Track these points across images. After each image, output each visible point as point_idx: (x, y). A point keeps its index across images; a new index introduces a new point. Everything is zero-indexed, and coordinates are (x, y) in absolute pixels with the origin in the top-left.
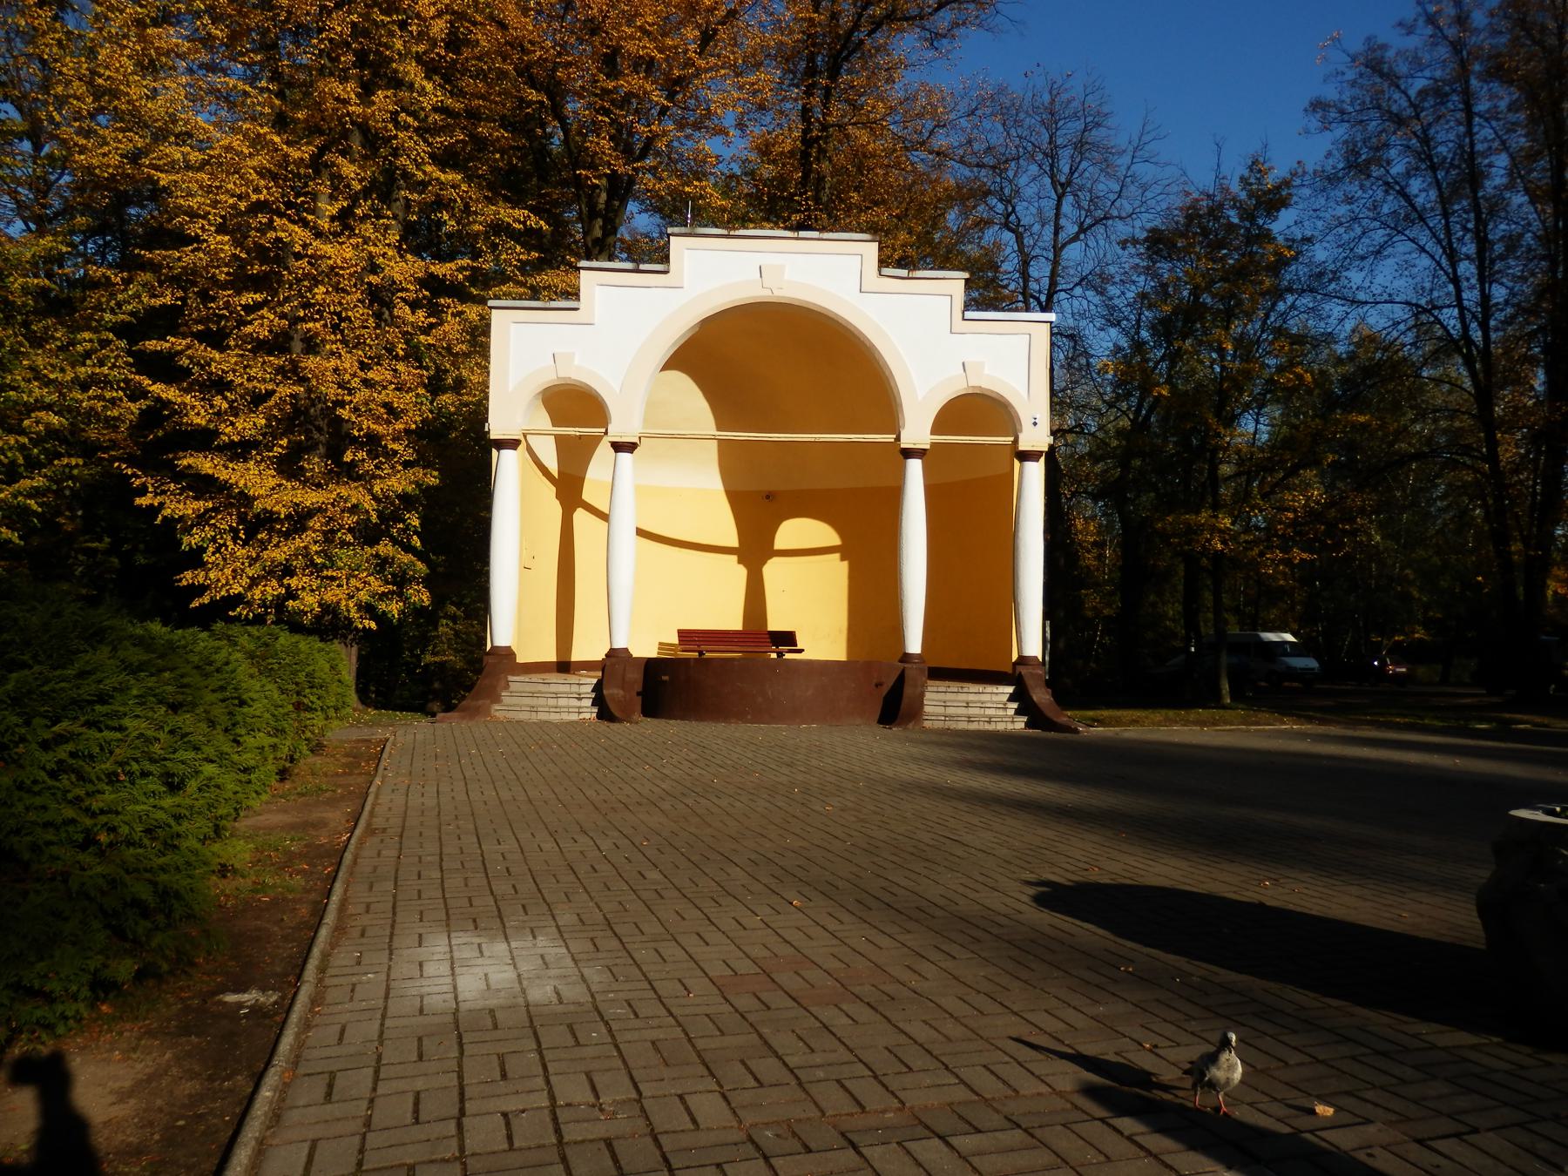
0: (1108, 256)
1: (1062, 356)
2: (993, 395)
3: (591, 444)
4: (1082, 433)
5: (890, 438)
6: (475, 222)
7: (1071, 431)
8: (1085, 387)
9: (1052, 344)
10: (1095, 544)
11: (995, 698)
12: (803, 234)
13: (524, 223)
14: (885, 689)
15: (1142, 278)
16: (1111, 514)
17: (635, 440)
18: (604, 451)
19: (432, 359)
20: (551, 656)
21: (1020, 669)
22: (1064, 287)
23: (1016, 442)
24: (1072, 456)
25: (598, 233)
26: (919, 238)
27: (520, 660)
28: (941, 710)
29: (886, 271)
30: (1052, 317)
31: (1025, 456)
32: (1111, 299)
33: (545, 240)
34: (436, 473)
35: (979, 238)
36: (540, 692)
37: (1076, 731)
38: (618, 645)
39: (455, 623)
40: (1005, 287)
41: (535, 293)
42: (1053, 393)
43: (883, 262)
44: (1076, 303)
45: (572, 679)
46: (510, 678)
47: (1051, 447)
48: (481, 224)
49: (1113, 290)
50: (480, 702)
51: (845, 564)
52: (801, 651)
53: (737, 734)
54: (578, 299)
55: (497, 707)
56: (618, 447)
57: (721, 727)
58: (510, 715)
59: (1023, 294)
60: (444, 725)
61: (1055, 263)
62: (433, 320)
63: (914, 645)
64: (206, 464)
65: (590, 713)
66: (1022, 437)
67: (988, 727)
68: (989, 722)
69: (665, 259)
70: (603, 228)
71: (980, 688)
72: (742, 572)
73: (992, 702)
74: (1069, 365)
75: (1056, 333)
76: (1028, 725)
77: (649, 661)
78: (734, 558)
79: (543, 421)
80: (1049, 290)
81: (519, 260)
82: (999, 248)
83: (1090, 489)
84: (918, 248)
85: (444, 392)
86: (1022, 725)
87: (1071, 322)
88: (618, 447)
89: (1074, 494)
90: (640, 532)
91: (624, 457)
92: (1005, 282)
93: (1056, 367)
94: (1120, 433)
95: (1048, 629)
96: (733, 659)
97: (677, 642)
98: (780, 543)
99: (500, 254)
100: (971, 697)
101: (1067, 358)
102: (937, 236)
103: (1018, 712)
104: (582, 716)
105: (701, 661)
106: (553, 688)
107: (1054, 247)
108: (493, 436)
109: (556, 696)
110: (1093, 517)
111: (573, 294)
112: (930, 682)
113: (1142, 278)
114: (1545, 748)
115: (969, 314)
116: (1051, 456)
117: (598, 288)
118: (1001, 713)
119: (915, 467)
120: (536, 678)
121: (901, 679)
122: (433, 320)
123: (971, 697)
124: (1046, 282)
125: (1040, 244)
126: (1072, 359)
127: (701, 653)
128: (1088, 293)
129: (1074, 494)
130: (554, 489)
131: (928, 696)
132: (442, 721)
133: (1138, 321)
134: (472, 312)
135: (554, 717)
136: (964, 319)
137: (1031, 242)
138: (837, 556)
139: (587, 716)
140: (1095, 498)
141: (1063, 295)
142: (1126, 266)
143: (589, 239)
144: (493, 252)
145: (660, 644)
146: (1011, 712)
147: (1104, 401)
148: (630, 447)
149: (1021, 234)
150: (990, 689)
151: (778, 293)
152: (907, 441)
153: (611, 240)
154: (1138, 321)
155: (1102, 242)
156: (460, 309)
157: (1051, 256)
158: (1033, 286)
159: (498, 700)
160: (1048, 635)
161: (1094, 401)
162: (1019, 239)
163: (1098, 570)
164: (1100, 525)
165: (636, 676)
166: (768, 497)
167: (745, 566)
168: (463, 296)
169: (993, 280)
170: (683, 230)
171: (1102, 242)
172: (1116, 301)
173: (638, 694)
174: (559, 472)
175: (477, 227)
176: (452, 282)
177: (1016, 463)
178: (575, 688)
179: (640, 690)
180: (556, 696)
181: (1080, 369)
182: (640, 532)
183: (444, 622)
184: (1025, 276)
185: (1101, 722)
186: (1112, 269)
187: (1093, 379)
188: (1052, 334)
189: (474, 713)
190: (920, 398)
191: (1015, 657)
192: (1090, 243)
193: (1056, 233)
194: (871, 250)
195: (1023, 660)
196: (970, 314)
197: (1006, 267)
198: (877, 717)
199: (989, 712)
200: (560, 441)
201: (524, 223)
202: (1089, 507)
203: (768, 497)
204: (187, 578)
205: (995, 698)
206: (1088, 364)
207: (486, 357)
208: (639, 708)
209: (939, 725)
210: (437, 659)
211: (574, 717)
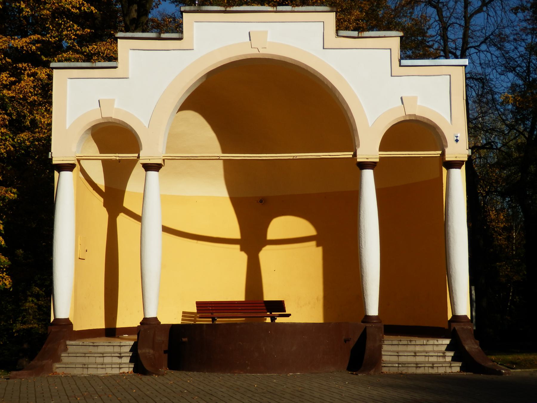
0: (504, 21)
1: (474, 94)
2: (425, 121)
3: (130, 165)
4: (491, 148)
5: (349, 154)
6: (44, 9)
7: (483, 147)
8: (492, 115)
9: (467, 85)
10: (504, 229)
11: (436, 348)
12: (280, 8)
13: (79, 9)
14: (352, 344)
15: (530, 36)
16: (516, 207)
17: (160, 162)
18: (138, 170)
19: (13, 108)
20: (101, 325)
22: (473, 44)
23: (443, 154)
24: (484, 165)
25: (134, 15)
26: (367, 13)
27: (76, 328)
28: (395, 359)
29: (342, 33)
30: (466, 61)
32: (507, 52)
33: (97, 21)
34: (14, 190)
35: (411, 13)
36: (91, 353)
37: (500, 373)
38: (151, 314)
39: (38, 300)
40: (431, 47)
41: (88, 58)
42: (469, 120)
43: (340, 26)
44: (482, 55)
45: (116, 342)
46: (68, 342)
47: (469, 157)
48: (48, 9)
49: (509, 46)
50: (45, 362)
51: (320, 249)
52: (288, 315)
53: (238, 383)
54: (116, 59)
55: (57, 365)
56: (148, 167)
57: (227, 376)
58: (68, 371)
59: (444, 51)
60: (16, 381)
61: (466, 28)
62: (13, 79)
65: (128, 368)
66: (447, 151)
67: (431, 371)
68: (433, 367)
70: (138, 11)
71: (424, 341)
72: (243, 257)
73: (434, 351)
74: (480, 101)
75: (470, 78)
76: (462, 369)
77: (173, 328)
78: (238, 247)
79: (93, 149)
80: (462, 47)
81: (76, 35)
82: (425, 19)
83: (499, 189)
84: (367, 21)
85: (23, 132)
86: (458, 369)
87: (479, 70)
88: (148, 167)
89: (488, 193)
90: (165, 229)
91: (152, 174)
92: (431, 43)
93: (470, 102)
94: (519, 147)
95: (473, 292)
96: (235, 324)
97: (195, 310)
98: (272, 234)
99: (62, 31)
100: (418, 348)
101: (478, 95)
102: (380, 13)
103: (454, 359)
104: (122, 371)
105: (213, 327)
106: (100, 349)
107: (465, 17)
108: (54, 162)
109: (103, 355)
110: (502, 209)
111: (113, 57)
112: (386, 337)
113: (530, 36)
115: (404, 62)
116: (469, 164)
118: (441, 359)
119: (368, 176)
120: (88, 341)
121: (364, 336)
122: (13, 79)
123: (418, 348)
124: (460, 42)
125: (455, 15)
126: (481, 95)
127: (214, 319)
128: (490, 49)
129: (488, 193)
130: (102, 200)
131: (385, 348)
132: (14, 378)
133: (528, 67)
134: (42, 73)
135: (101, 372)
136: (400, 66)
137: (448, 14)
138: (314, 243)
139: (126, 370)
140: (503, 195)
141: (473, 50)
142: (518, 28)
143: (127, 19)
144: (57, 30)
145: (184, 313)
146: (449, 359)
147: (507, 125)
148: (156, 167)
149: (441, 9)
150: (432, 341)
151: (262, 51)
153: (144, 19)
154: (528, 67)
155: (499, 12)
156: (33, 70)
157: (463, 23)
158: (451, 45)
159: (58, 360)
160: (474, 297)
161: (499, 124)
162: (440, 12)
163: (508, 247)
164: (508, 215)
165: (163, 339)
166: (261, 201)
167: (246, 252)
168: (37, 62)
169: (422, 42)
170: (192, 8)
171: (499, 12)
172: (512, 54)
173: (165, 352)
174: (106, 187)
175: (45, 12)
176: (27, 51)
177: (444, 170)
178: (117, 349)
179: (166, 348)
180: (103, 355)
181: (487, 103)
182: (165, 229)
183: (30, 299)
184: (445, 38)
185: (519, 365)
186: (508, 31)
187: (497, 110)
188: (466, 79)
189: (39, 370)
191: (450, 316)
192: (490, 13)
193: (466, 7)
194: (330, 18)
195: (456, 318)
196: (404, 62)
197: (431, 32)
198: (346, 365)
199: (432, 359)
200: (106, 164)
201: (79, 9)
202: (500, 202)
203: (261, 201)
205: (436, 348)
206: (494, 100)
207: (51, 104)
208: (165, 362)
209: (393, 370)
210: (25, 327)
211: (116, 371)
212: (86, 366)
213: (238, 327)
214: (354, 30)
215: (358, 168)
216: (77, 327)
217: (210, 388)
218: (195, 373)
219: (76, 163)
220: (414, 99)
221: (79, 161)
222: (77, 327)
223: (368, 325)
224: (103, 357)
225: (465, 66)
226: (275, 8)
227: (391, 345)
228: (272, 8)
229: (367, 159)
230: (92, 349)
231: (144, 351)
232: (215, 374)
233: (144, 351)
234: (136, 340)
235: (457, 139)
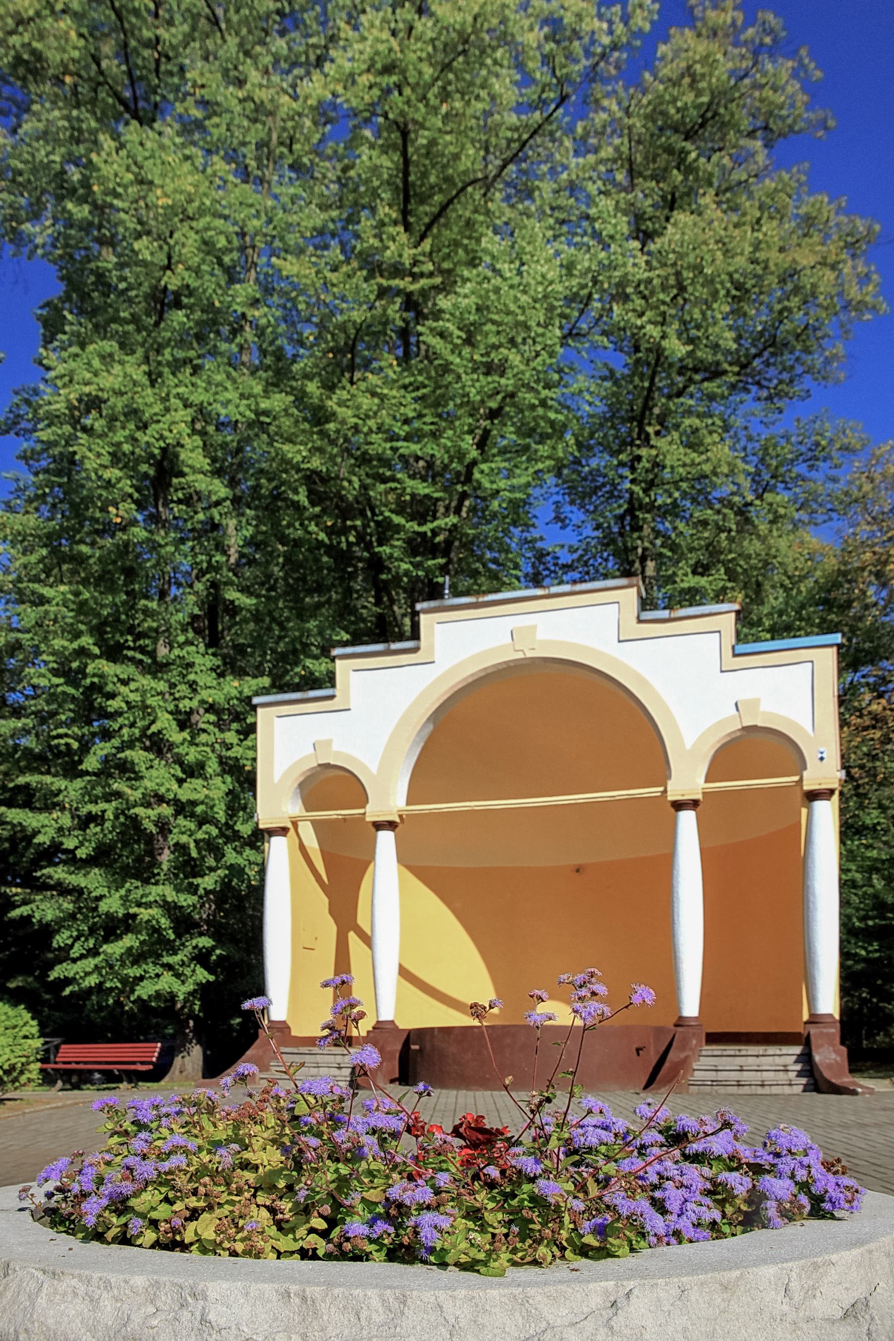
5: (657, 790)
30: (838, 638)
31: (813, 796)
54: (333, 686)
63: (690, 1007)
64: (59, 873)
69: (415, 635)
103: (800, 1074)
111: (330, 679)
136: (640, 621)
151: (530, 654)
152: (374, 811)
178: (339, 1059)
190: (688, 745)
191: (806, 1017)
194: (629, 597)
195: (815, 1019)
200: (317, 825)
204: (56, 973)
214: (665, 608)
215: (672, 810)
219: (290, 825)
220: (756, 702)
221: (295, 824)
230: (307, 1058)
234: (296, 1032)
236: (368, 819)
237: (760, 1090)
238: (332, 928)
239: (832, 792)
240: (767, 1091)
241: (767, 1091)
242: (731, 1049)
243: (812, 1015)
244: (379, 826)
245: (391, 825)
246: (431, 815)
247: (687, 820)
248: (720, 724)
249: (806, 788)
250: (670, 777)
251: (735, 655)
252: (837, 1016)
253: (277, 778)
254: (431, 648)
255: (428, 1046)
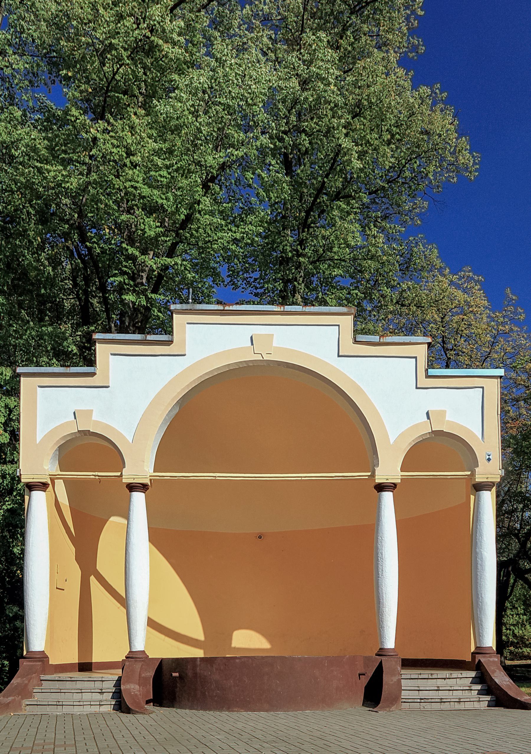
20: (74, 659)
21: (479, 657)
30: (501, 372)
31: (479, 487)
45: (95, 675)
53: (240, 725)
57: (224, 715)
63: (390, 643)
103: (481, 692)
114: (90, 475)
115: (432, 372)
117: (111, 357)
135: (77, 710)
136: (356, 342)
178: (98, 685)
190: (392, 441)
191: (473, 649)
194: (347, 322)
200: (68, 483)
203: (260, 537)
212: (61, 703)
213: (237, 661)
216: (53, 661)
217: (204, 734)
218: (187, 711)
219: (49, 482)
220: (443, 413)
222: (53, 661)
223: (383, 658)
224: (81, 692)
225: (501, 377)
226: (282, 308)
227: (410, 679)
228: (279, 307)
229: (387, 479)
231: (128, 686)
232: (211, 713)
233: (128, 686)
235: (489, 458)
236: (124, 481)
237: (457, 706)
238: (76, 572)
239: (493, 484)
240: (462, 706)
241: (462, 706)
242: (425, 673)
243: (477, 648)
244: (132, 488)
245: (143, 488)
246: (435, 479)
247: (388, 497)
248: (416, 426)
249: (377, 481)
250: (378, 465)
251: (428, 376)
252: (494, 648)
253: (39, 438)
254: (183, 342)
255: (190, 674)
